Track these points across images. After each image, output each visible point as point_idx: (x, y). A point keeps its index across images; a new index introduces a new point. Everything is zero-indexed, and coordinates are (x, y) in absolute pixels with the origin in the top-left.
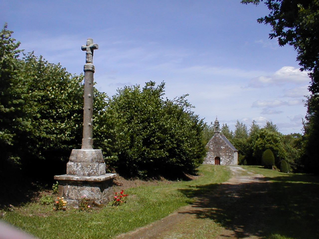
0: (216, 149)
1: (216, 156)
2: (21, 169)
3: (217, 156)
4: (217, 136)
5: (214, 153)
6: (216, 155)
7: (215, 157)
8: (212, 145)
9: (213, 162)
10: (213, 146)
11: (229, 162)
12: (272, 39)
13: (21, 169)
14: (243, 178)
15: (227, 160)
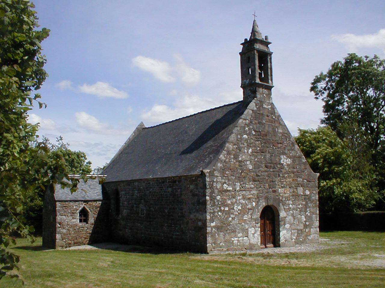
0: (263, 169)
1: (264, 204)
2: (22, 77)
3: (270, 203)
4: (265, 106)
5: (257, 187)
6: (267, 199)
7: (261, 209)
8: (249, 146)
9: (254, 235)
10: (252, 154)
11: (306, 226)
12: (47, 107)
13: (22, 77)
14: (305, 255)
15: (300, 221)
